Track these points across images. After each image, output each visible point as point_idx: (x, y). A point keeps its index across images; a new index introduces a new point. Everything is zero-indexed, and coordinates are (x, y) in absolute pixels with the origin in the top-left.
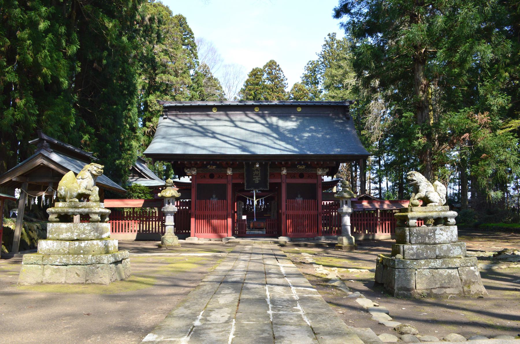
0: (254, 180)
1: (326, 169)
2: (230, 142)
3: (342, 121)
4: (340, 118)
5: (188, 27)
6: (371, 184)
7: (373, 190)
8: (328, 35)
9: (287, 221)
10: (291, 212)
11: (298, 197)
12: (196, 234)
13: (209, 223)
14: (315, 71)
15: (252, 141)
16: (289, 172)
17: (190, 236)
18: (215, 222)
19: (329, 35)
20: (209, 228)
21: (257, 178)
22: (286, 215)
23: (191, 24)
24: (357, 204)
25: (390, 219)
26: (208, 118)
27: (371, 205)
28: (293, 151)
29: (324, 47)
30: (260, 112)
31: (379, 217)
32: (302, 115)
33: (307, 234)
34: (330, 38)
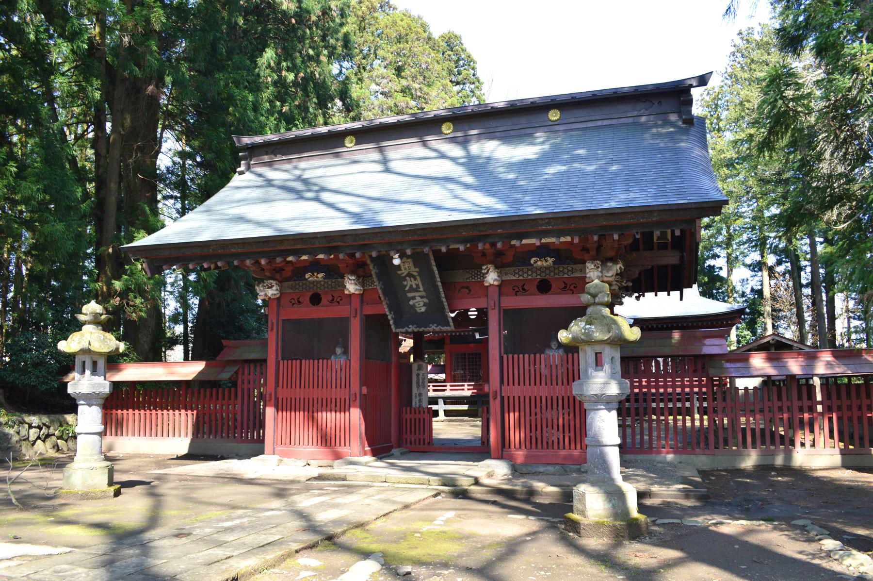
0: (411, 303)
1: (616, 262)
2: (341, 206)
3: (672, 130)
4: (667, 123)
5: (464, 50)
6: (852, 320)
7: (856, 332)
8: (738, 34)
9: (506, 415)
10: (515, 391)
11: (550, 347)
12: (279, 448)
13: (313, 420)
14: (717, 105)
15: (404, 197)
16: (505, 278)
17: (262, 452)
18: (328, 418)
19: (740, 33)
20: (312, 433)
21: (418, 299)
22: (502, 398)
23: (471, 46)
24: (728, 365)
25: (835, 407)
26: (340, 161)
27: (775, 367)
28: (488, 209)
29: (732, 58)
30: (459, 134)
31: (819, 398)
32: (561, 128)
33: (563, 453)
34: (742, 38)
